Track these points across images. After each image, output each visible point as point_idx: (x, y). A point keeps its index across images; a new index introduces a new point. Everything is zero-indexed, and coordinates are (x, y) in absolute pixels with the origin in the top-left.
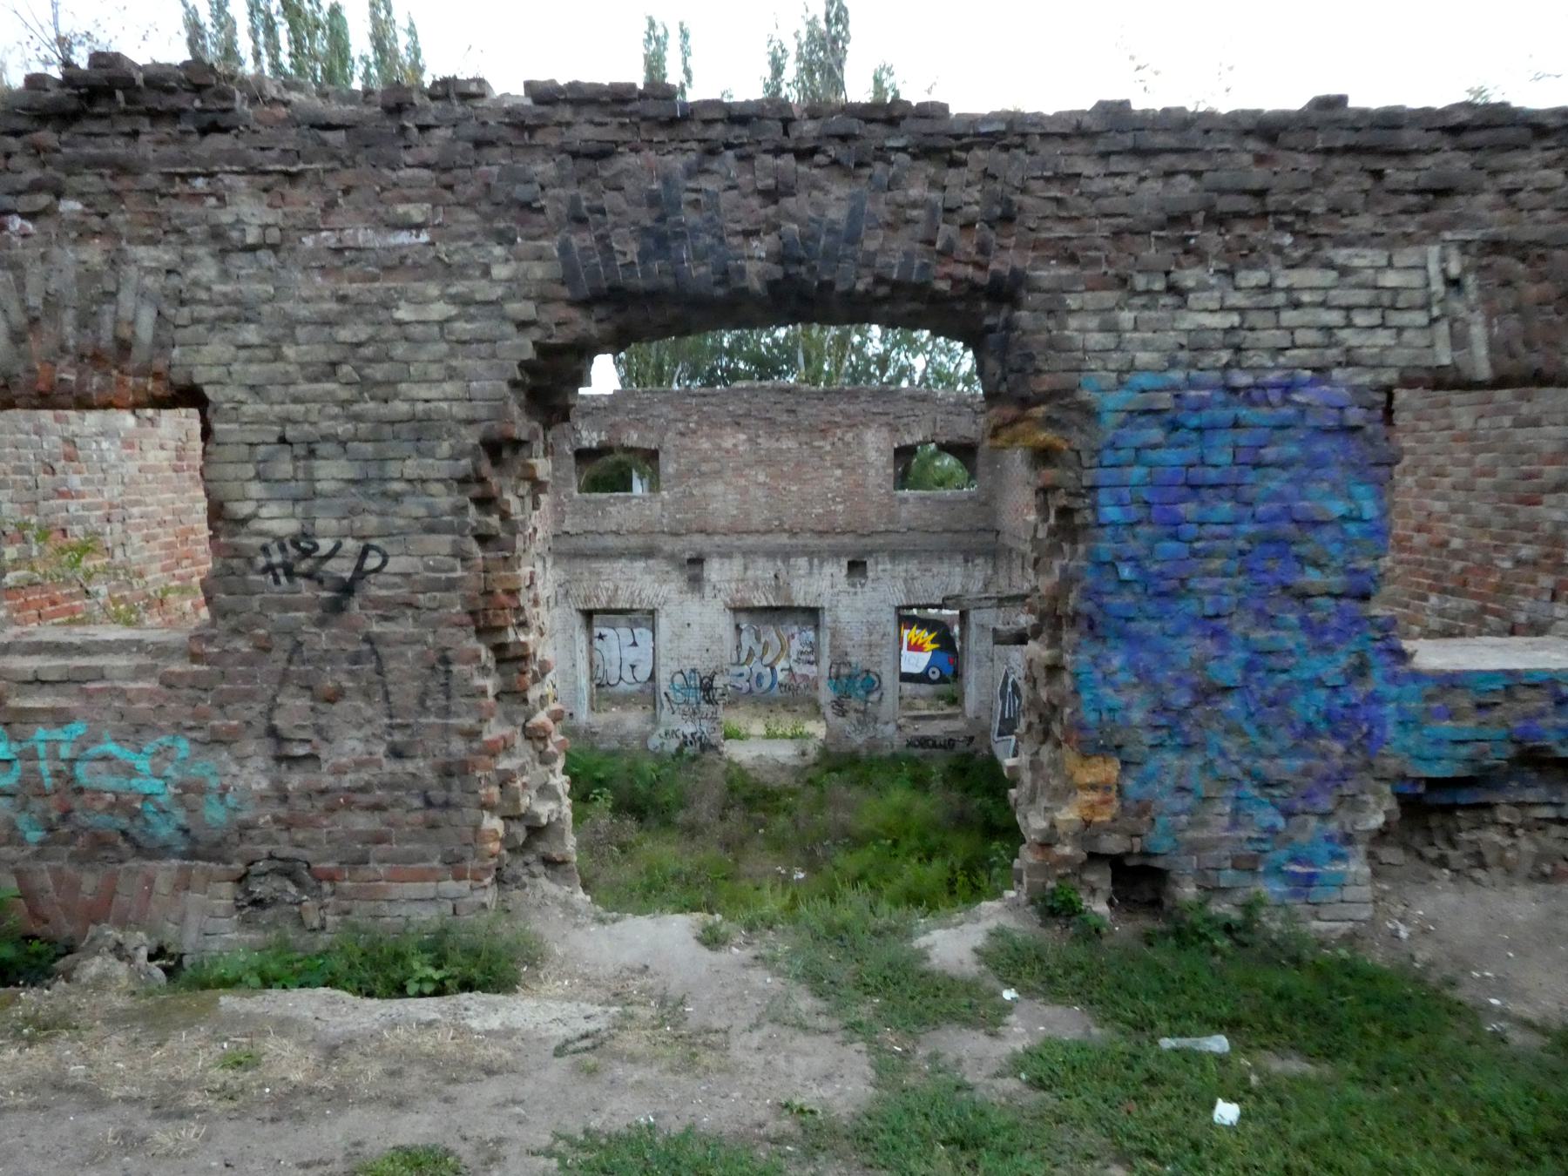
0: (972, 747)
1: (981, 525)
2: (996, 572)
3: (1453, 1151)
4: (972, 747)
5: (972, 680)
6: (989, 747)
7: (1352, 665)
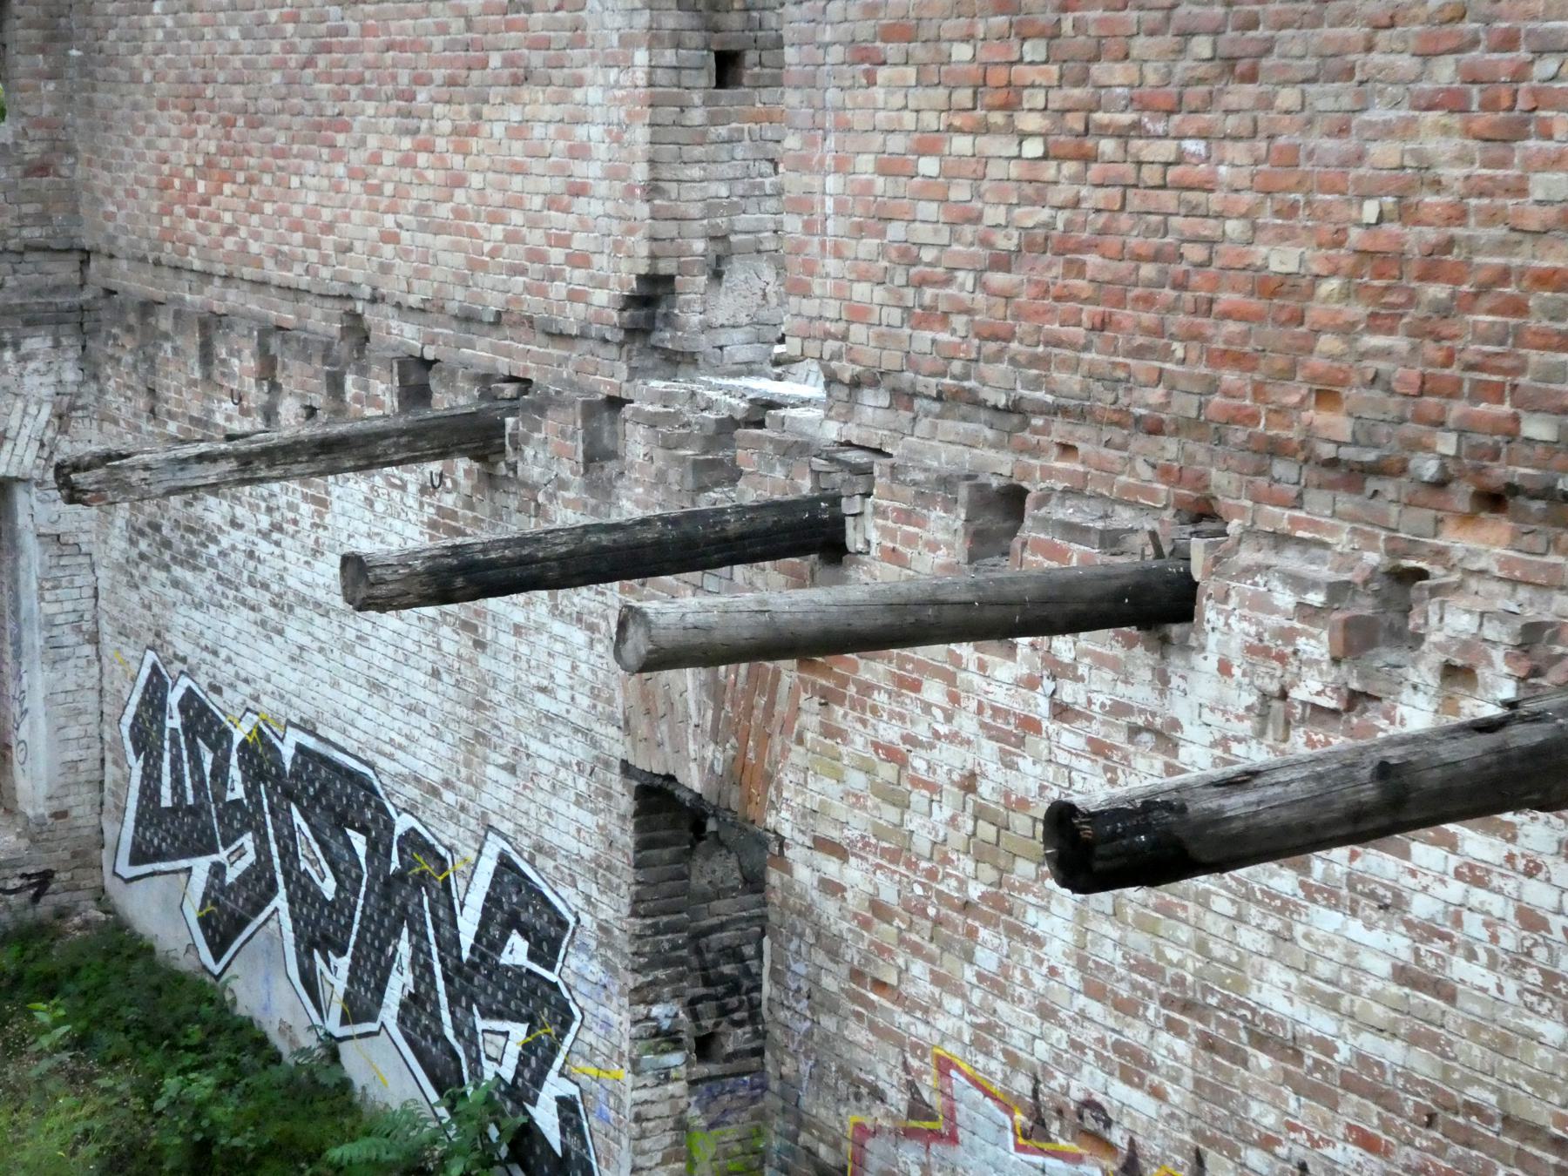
0: (45, 907)
1: (34, 233)
2: (91, 370)
3: (1359, 1164)
4: (45, 907)
5: (36, 701)
6: (101, 896)
7: (1012, 872)
